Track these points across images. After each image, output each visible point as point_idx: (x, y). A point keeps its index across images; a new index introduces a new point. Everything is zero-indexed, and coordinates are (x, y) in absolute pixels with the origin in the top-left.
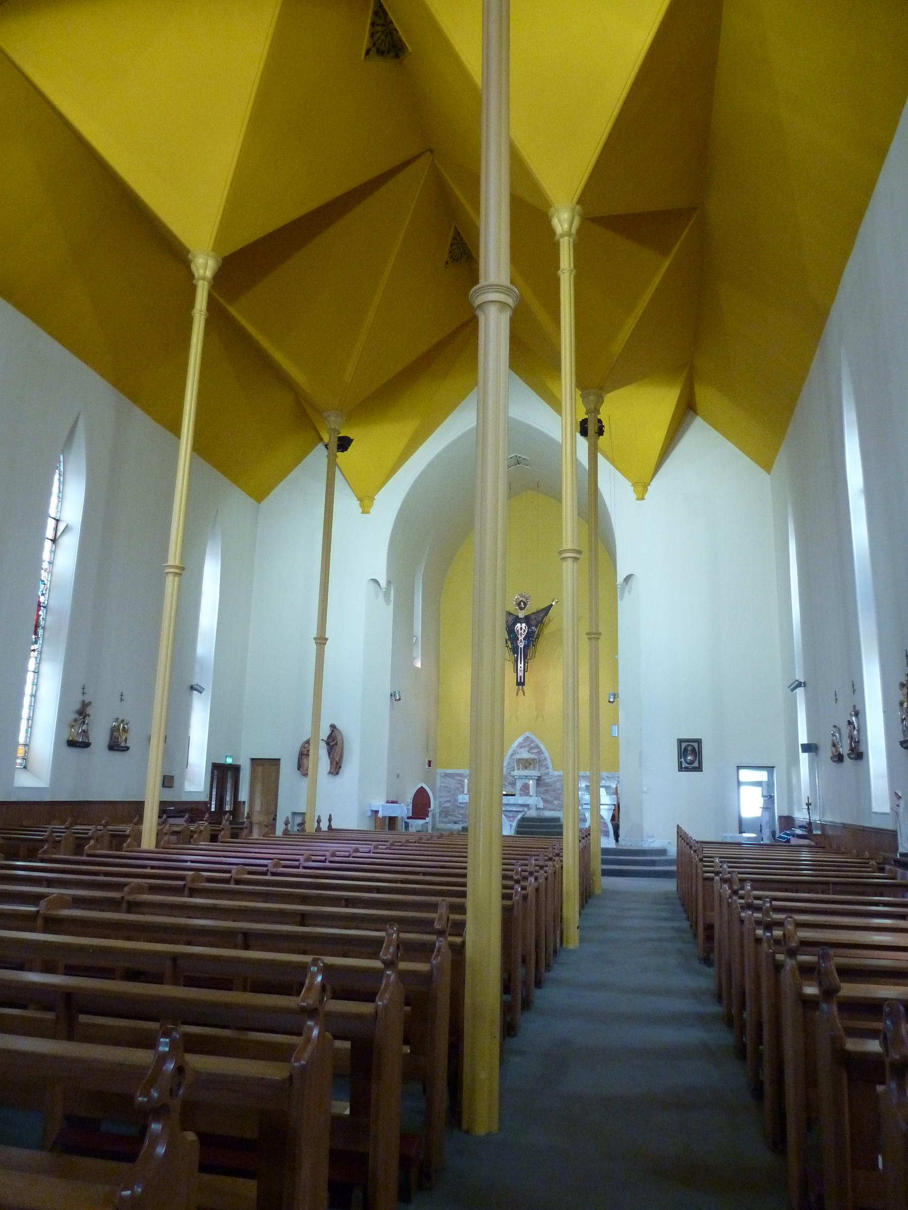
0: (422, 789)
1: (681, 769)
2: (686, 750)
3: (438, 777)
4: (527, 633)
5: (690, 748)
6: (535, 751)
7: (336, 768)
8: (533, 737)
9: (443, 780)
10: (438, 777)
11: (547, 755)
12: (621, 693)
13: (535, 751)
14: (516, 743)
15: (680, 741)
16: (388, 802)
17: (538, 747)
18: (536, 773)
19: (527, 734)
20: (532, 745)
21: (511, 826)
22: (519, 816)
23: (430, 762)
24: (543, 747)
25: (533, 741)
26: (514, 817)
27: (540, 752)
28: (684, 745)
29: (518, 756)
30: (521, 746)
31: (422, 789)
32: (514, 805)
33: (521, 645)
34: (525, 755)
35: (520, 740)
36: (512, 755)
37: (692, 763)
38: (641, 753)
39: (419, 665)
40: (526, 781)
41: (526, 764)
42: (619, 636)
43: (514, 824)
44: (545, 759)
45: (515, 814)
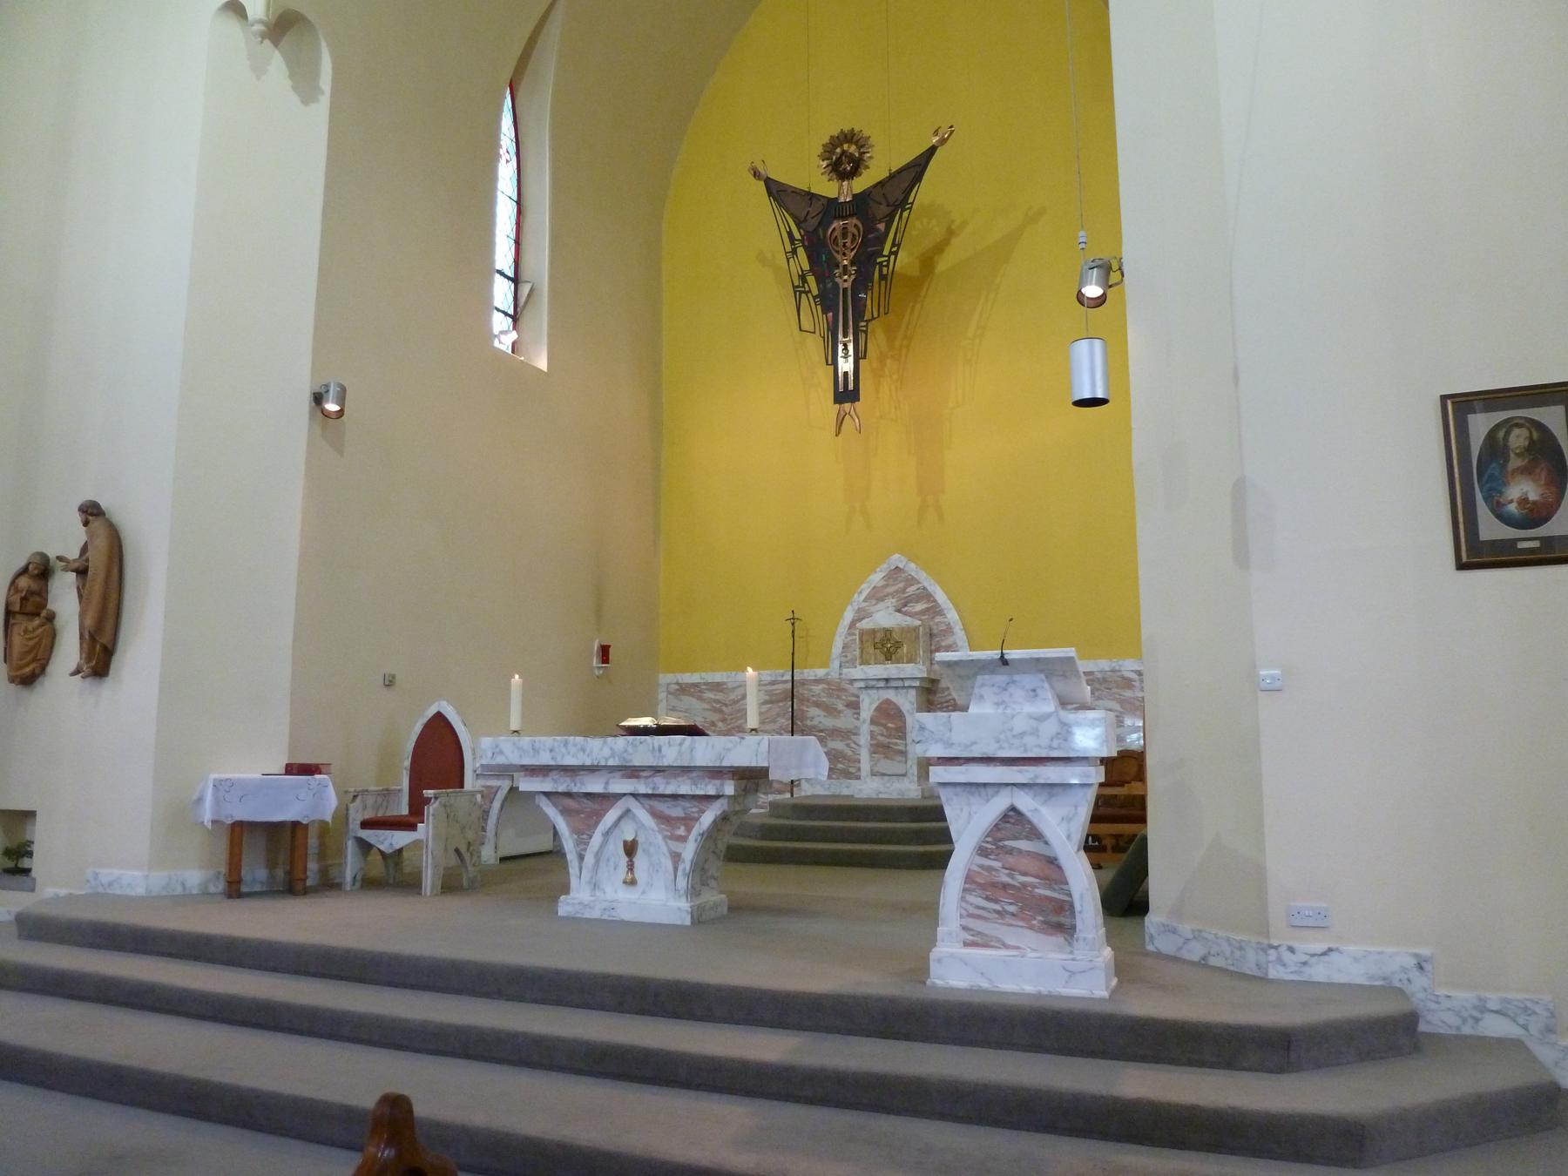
0: (439, 717)
1: (1475, 555)
2: (1495, 447)
3: (662, 695)
4: (853, 248)
5: (1518, 439)
6: (919, 607)
7: (100, 659)
8: (912, 568)
9: (674, 702)
10: (662, 695)
11: (952, 616)
12: (1133, 253)
13: (919, 607)
14: (866, 589)
15: (1459, 406)
16: (290, 769)
17: (926, 595)
18: (915, 670)
19: (897, 559)
20: (911, 590)
21: (676, 858)
22: (708, 818)
23: (605, 653)
24: (941, 597)
25: (911, 581)
26: (689, 821)
27: (935, 610)
28: (1481, 424)
29: (866, 624)
30: (877, 596)
31: (439, 717)
32: (686, 770)
33: (845, 282)
34: (885, 617)
35: (877, 578)
36: (852, 625)
37: (1535, 515)
38: (1239, 491)
39: (542, 364)
40: (890, 695)
41: (886, 646)
42: (1112, 22)
43: (689, 851)
44: (949, 630)
45: (692, 808)
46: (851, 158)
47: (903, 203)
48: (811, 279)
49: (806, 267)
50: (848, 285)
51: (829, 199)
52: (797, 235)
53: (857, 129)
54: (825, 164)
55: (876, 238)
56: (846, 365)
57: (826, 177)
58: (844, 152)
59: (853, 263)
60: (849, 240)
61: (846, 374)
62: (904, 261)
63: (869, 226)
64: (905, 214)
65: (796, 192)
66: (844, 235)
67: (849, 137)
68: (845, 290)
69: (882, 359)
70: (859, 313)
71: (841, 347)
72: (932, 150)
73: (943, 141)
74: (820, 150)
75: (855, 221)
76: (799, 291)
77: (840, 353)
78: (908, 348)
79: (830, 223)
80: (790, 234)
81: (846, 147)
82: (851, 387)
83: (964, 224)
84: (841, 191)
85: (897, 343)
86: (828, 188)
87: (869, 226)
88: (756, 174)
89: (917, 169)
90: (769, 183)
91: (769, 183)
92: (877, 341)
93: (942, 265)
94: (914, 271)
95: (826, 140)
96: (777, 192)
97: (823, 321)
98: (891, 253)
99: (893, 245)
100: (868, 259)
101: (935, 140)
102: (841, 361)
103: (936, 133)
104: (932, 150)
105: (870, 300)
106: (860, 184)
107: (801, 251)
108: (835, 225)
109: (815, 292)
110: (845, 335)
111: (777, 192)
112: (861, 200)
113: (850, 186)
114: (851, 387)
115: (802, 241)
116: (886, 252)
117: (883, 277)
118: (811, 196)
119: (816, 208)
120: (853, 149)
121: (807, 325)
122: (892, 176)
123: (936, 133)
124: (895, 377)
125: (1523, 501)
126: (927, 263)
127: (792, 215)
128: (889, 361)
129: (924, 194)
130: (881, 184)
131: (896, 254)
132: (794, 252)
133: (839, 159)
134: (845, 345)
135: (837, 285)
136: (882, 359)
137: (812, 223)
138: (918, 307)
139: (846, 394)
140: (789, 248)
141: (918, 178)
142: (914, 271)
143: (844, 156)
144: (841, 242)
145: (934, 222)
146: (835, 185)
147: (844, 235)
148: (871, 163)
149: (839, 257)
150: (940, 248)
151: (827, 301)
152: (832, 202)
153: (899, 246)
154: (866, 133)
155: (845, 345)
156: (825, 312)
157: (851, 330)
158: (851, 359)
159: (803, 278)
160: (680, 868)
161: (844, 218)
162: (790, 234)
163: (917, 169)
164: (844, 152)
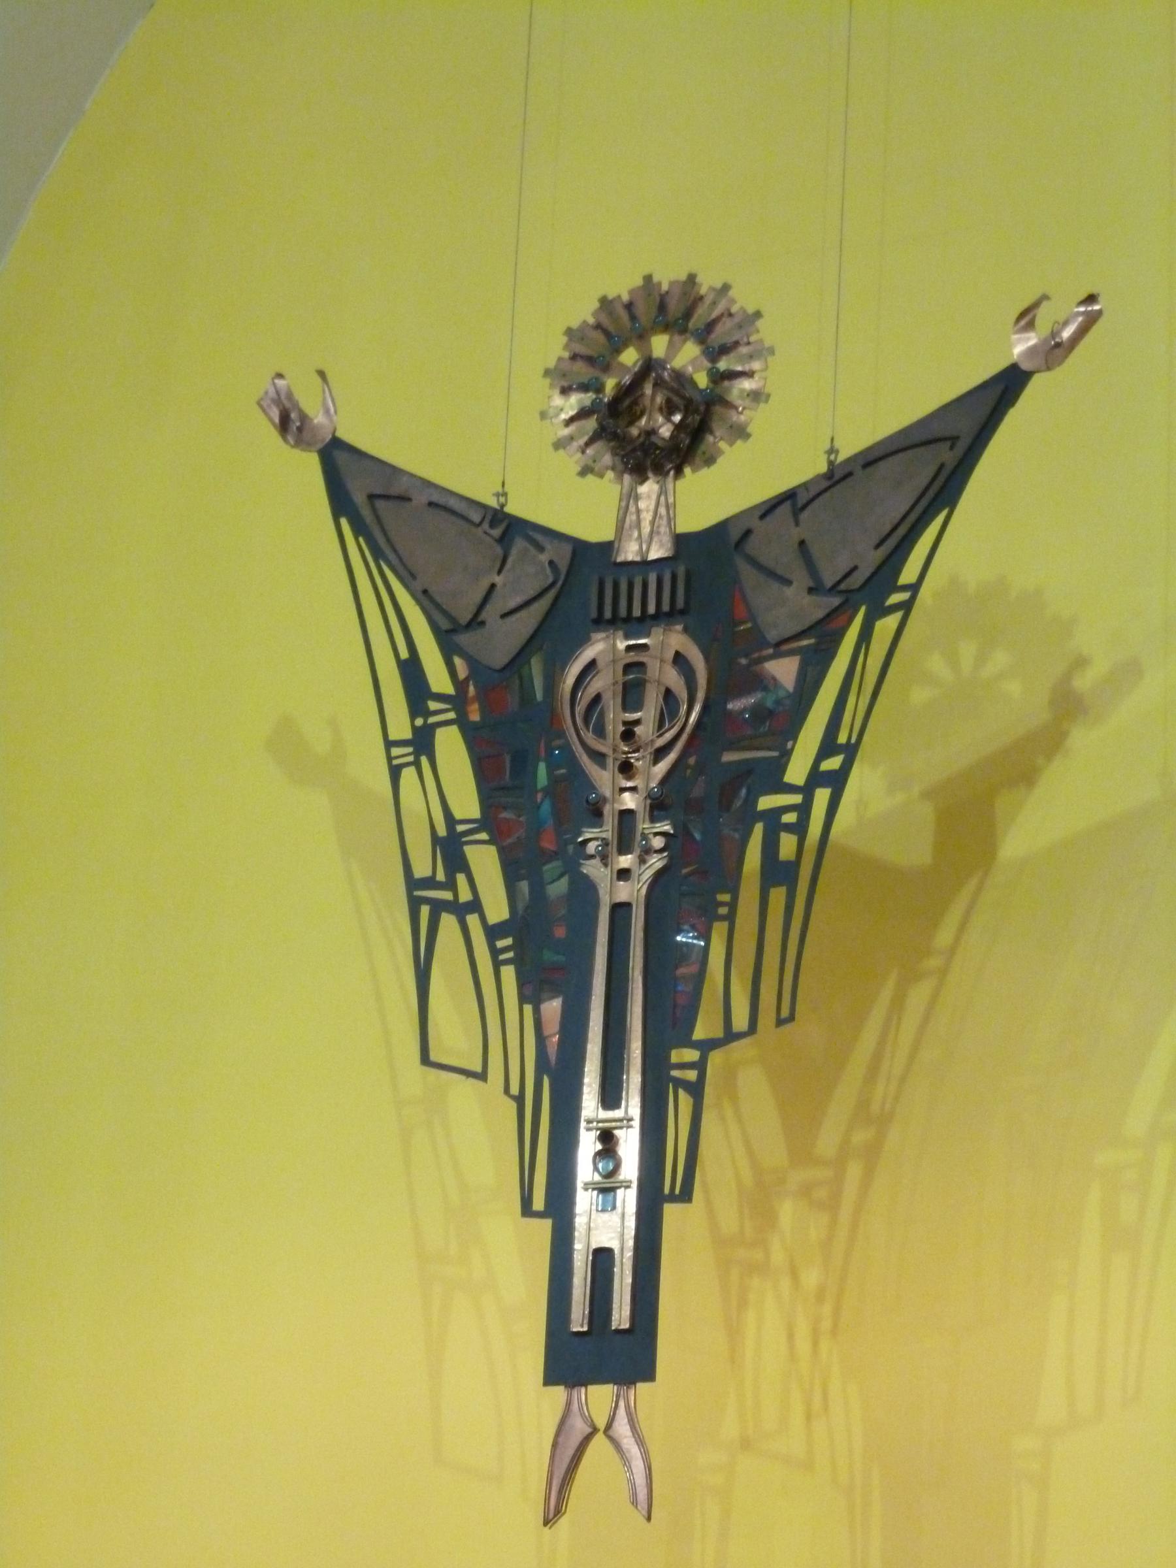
33: (624, 880)
46: (679, 392)
47: (876, 587)
48: (484, 861)
49: (467, 806)
50: (632, 892)
51: (581, 550)
52: (439, 679)
53: (707, 282)
54: (573, 403)
55: (760, 714)
56: (605, 1224)
57: (570, 461)
58: (649, 366)
59: (657, 807)
60: (648, 714)
61: (602, 1258)
62: (877, 808)
63: (734, 654)
64: (887, 625)
65: (445, 506)
66: (632, 694)
67: (673, 308)
68: (620, 910)
69: (760, 1202)
70: (670, 1020)
71: (588, 1144)
72: (1009, 384)
73: (1055, 352)
74: (555, 349)
75: (676, 639)
76: (430, 901)
77: (585, 1169)
78: (872, 1154)
79: (583, 641)
80: (411, 671)
81: (659, 344)
82: (621, 1315)
83: (1129, 672)
84: (646, 519)
85: (827, 1142)
86: (580, 502)
87: (734, 654)
88: (289, 422)
89: (944, 453)
90: (337, 459)
91: (337, 459)
92: (741, 1121)
93: (1031, 829)
94: (913, 849)
95: (584, 312)
96: (367, 497)
97: (519, 1030)
98: (816, 778)
99: (828, 747)
100: (725, 791)
101: (1020, 346)
102: (584, 1201)
103: (1026, 318)
104: (1009, 384)
105: (722, 958)
106: (708, 496)
107: (450, 745)
108: (596, 648)
109: (497, 909)
110: (610, 1096)
111: (367, 497)
112: (707, 569)
113: (440, 697)
114: (621, 1315)
115: (458, 701)
116: (797, 772)
117: (777, 872)
118: (507, 529)
119: (526, 576)
120: (686, 357)
121: (455, 1035)
122: (837, 477)
123: (1026, 318)
124: (811, 1278)
125: (651, 432)
126: (968, 819)
127: (424, 598)
128: (787, 1211)
129: (963, 550)
130: (791, 502)
131: (837, 781)
132: (423, 742)
133: (629, 392)
134: (607, 1138)
135: (585, 890)
136: (760, 1202)
137: (502, 639)
138: (918, 995)
139: (600, 1342)
140: (401, 728)
141: (945, 491)
142: (913, 849)
143: (651, 388)
144: (614, 717)
145: (1000, 659)
146: (606, 490)
147: (632, 694)
148: (757, 419)
149: (604, 779)
150: (1020, 764)
151: (543, 950)
152: (589, 559)
153: (851, 751)
154: (744, 299)
155: (607, 1138)
156: (533, 989)
157: (634, 1080)
158: (628, 1199)
159: (451, 848)
160: (739, 368)
161: (633, 624)
162: (411, 671)
163: (944, 453)
164: (649, 366)
